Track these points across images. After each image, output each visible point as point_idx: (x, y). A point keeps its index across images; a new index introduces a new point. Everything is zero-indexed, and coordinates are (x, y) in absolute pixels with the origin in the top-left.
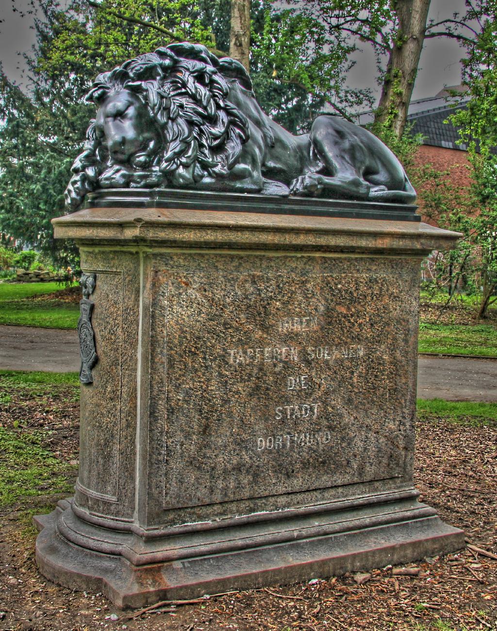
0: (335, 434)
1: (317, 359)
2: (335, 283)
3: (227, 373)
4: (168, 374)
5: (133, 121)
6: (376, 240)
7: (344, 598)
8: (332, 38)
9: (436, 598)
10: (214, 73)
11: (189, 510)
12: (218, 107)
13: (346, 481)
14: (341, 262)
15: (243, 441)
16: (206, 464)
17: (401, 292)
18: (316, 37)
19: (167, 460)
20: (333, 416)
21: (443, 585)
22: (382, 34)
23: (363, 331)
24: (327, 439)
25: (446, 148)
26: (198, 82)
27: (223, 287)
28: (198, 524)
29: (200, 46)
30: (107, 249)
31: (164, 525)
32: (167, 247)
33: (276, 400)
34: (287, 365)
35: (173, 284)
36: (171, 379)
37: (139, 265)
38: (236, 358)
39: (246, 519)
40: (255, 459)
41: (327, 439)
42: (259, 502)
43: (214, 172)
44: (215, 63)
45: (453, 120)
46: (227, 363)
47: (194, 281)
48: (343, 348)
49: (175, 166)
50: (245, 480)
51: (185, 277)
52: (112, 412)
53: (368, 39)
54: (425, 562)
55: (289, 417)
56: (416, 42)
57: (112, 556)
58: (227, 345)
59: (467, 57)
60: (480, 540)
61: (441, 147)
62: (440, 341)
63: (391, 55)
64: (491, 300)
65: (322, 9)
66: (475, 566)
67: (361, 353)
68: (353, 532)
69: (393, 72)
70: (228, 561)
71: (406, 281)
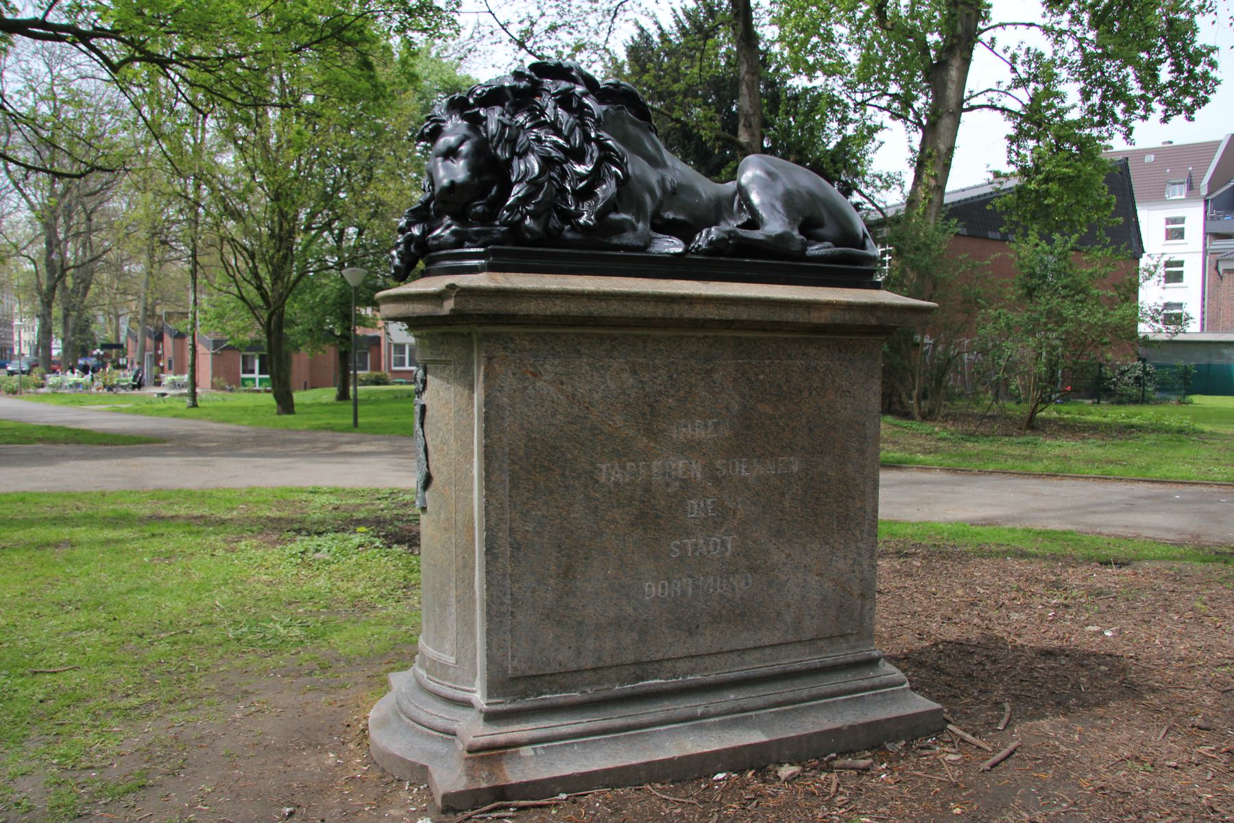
0: (758, 577)
1: (730, 475)
3: (597, 495)
4: (510, 496)
6: (809, 312)
7: (755, 803)
8: (857, 116)
9: (884, 809)
10: (584, 95)
11: (548, 678)
13: (776, 641)
14: (764, 344)
15: (622, 587)
16: (569, 617)
18: (839, 116)
19: (512, 613)
21: (900, 787)
22: (913, 110)
24: (747, 584)
25: (993, 239)
27: (589, 379)
28: (561, 697)
31: (511, 698)
32: (503, 324)
34: (686, 484)
35: (514, 374)
36: (515, 503)
37: (472, 351)
38: (610, 475)
39: (629, 691)
40: (641, 611)
41: (747, 584)
45: (998, 205)
46: (597, 482)
47: (546, 370)
48: (768, 461)
49: (519, 216)
51: (531, 365)
53: (899, 117)
54: (885, 749)
55: (690, 554)
56: (952, 117)
57: (446, 736)
58: (596, 456)
59: (1013, 132)
60: (967, 718)
61: (987, 238)
62: (977, 455)
63: (924, 132)
64: (1039, 408)
65: (845, 84)
66: (953, 757)
67: (795, 468)
68: (783, 708)
69: (927, 151)
71: (861, 370)
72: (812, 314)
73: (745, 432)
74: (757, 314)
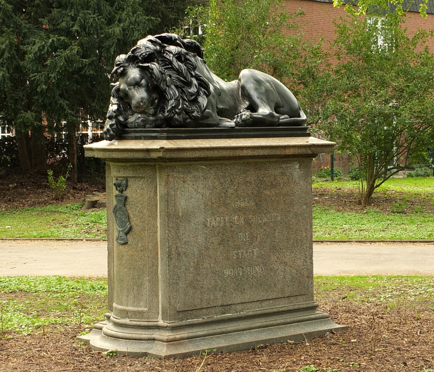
2: (262, 177)
5: (145, 88)
6: (285, 150)
12: (192, 76)
14: (265, 164)
23: (280, 205)
26: (178, 61)
28: (195, 321)
30: (136, 164)
31: (177, 321)
33: (233, 247)
38: (211, 223)
42: (226, 308)
43: (193, 116)
49: (173, 115)
50: (219, 294)
55: (240, 257)
70: (214, 340)
72: (286, 151)
73: (259, 203)
74: (266, 152)
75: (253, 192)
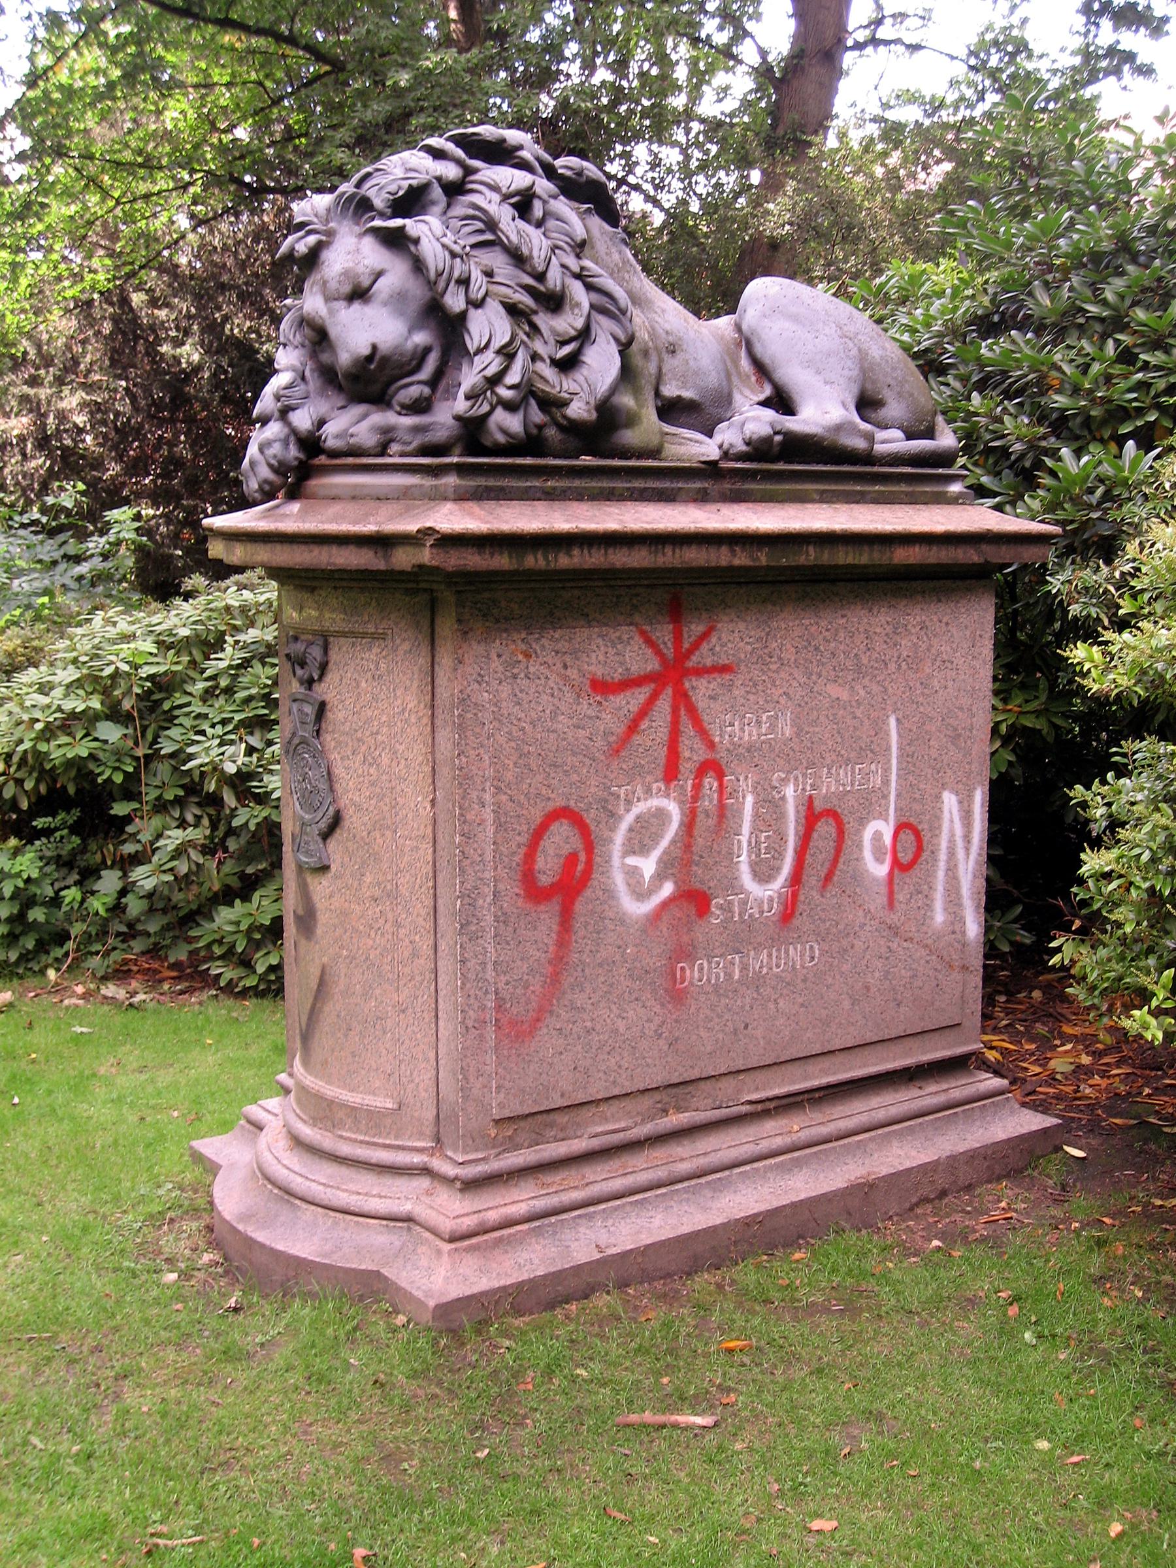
17: (956, 651)
20: (823, 910)
29: (514, 136)
35: (499, 656)
41: (813, 958)
44: (550, 172)
49: (486, 408)
52: (376, 926)
75: (791, 691)
